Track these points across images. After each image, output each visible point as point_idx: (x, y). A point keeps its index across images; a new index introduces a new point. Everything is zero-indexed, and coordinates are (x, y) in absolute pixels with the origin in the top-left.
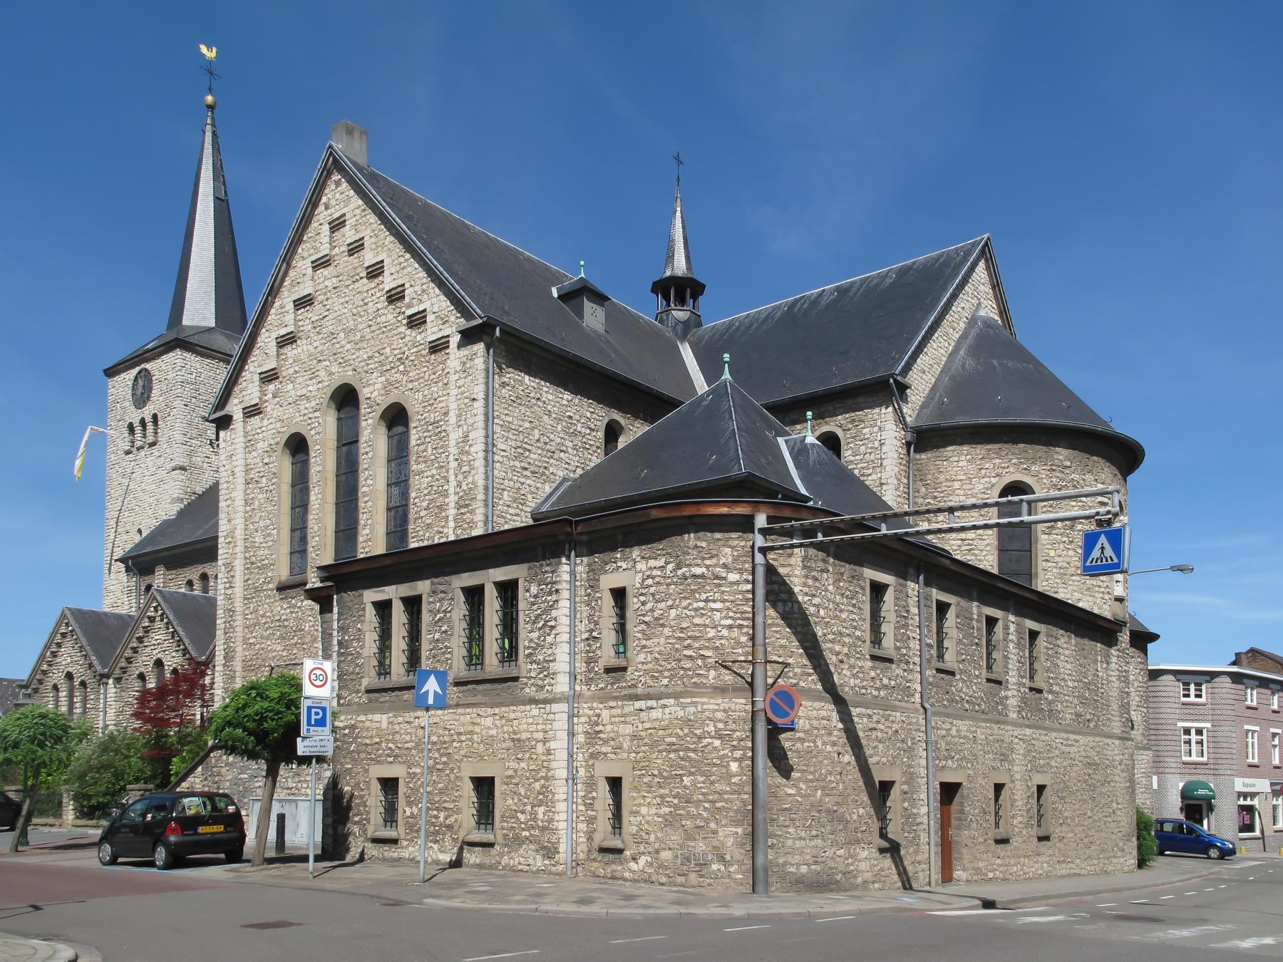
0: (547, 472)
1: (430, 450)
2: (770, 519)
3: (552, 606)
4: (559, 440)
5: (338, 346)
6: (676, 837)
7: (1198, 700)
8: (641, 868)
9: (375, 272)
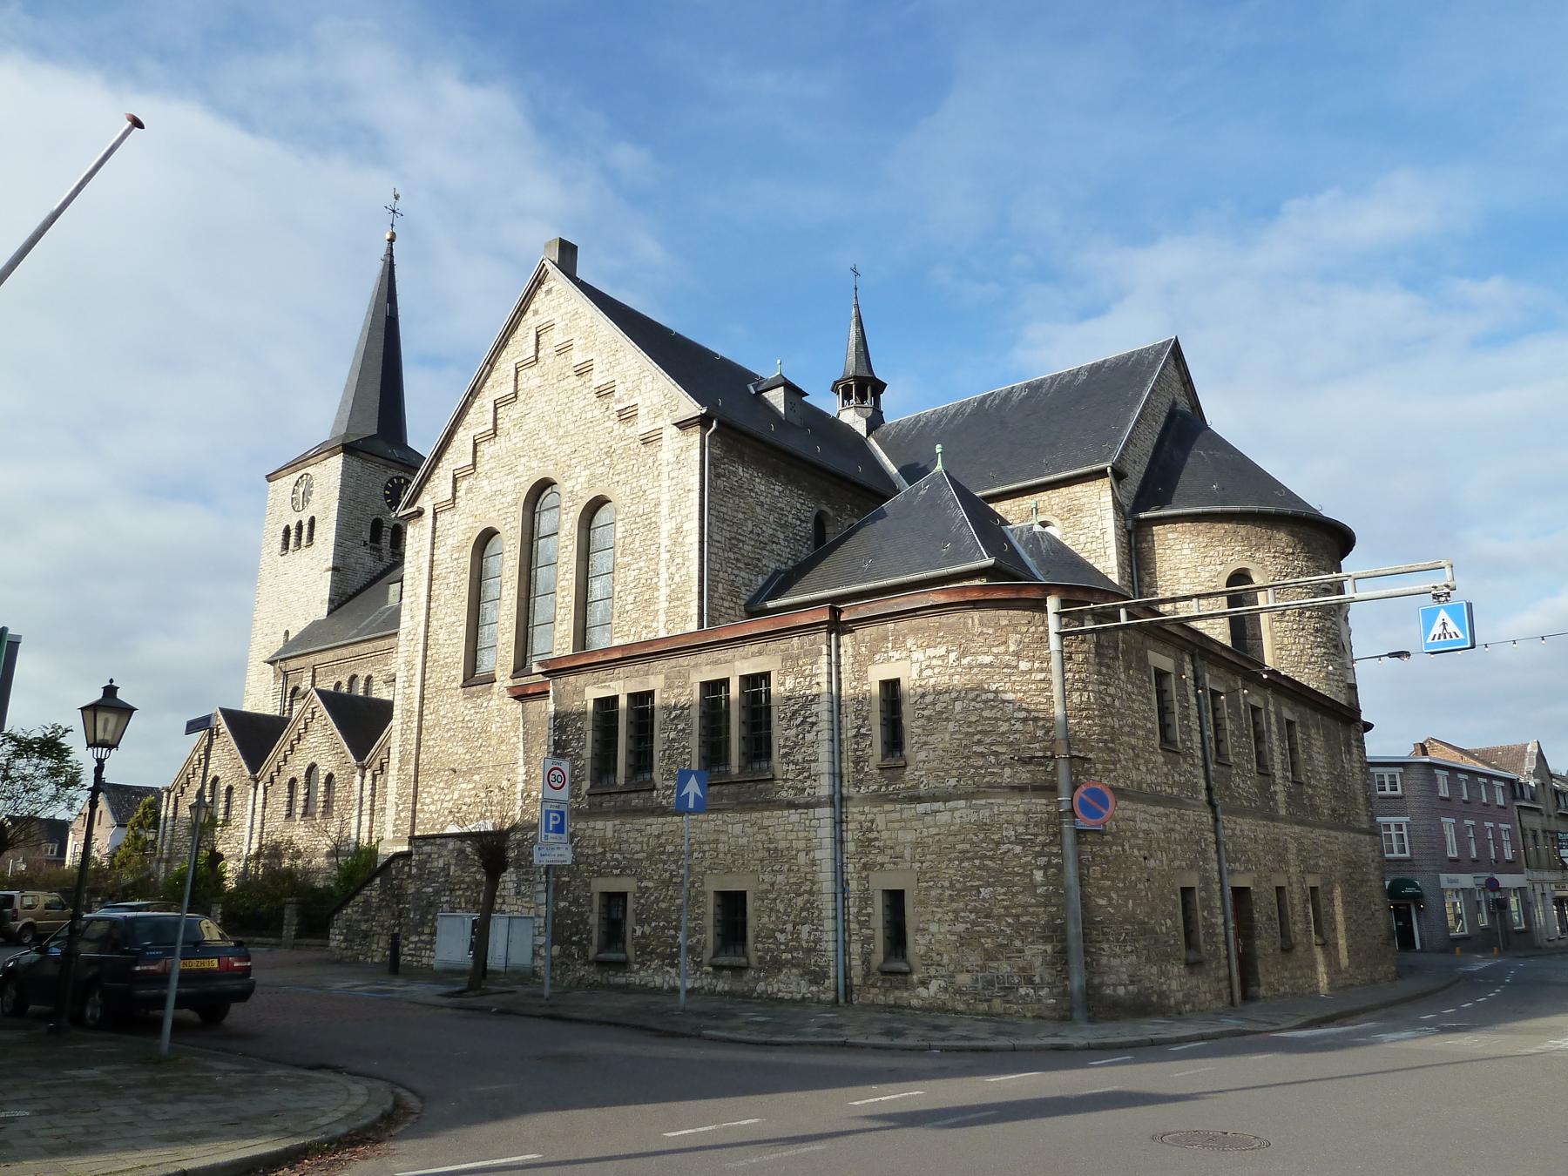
0: (760, 564)
1: (637, 543)
2: (1064, 603)
3: (811, 701)
4: (771, 532)
5: (539, 442)
6: (974, 959)
7: (1394, 793)
8: (932, 994)
9: (582, 371)
